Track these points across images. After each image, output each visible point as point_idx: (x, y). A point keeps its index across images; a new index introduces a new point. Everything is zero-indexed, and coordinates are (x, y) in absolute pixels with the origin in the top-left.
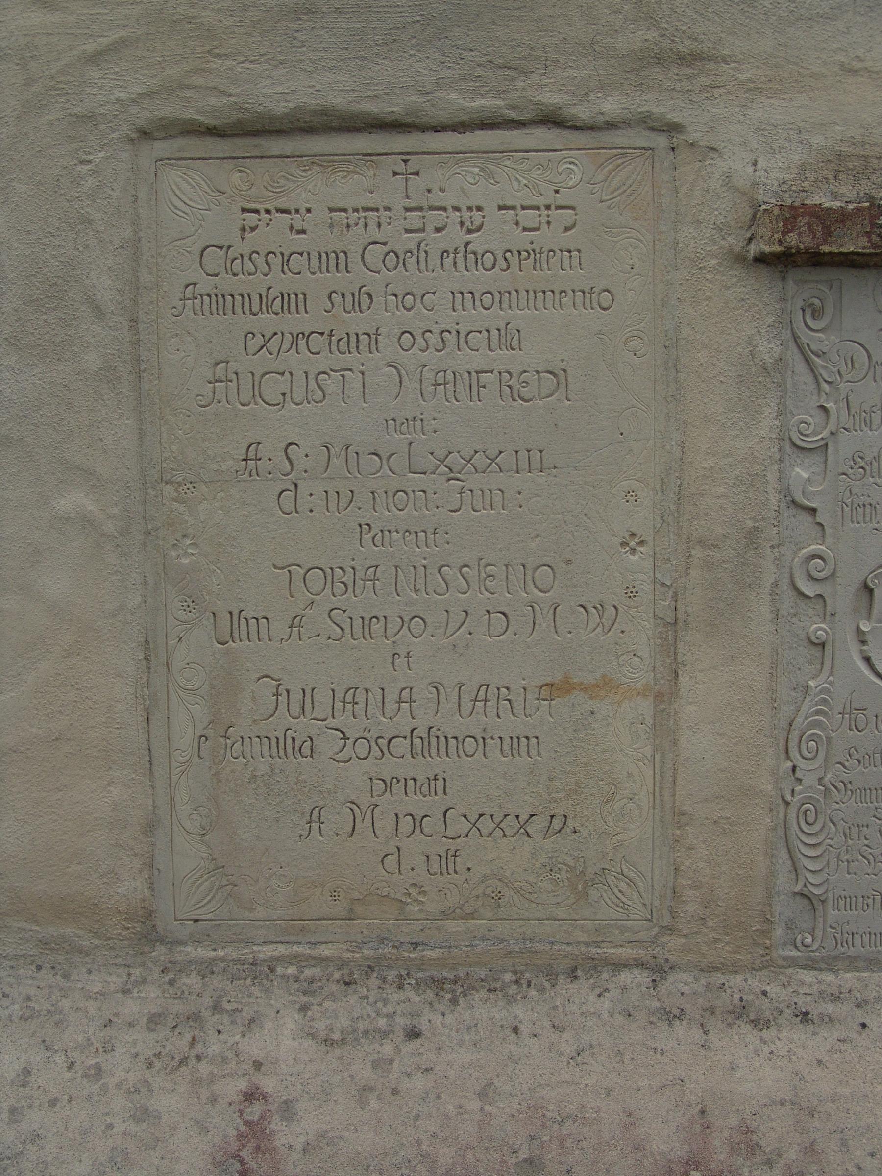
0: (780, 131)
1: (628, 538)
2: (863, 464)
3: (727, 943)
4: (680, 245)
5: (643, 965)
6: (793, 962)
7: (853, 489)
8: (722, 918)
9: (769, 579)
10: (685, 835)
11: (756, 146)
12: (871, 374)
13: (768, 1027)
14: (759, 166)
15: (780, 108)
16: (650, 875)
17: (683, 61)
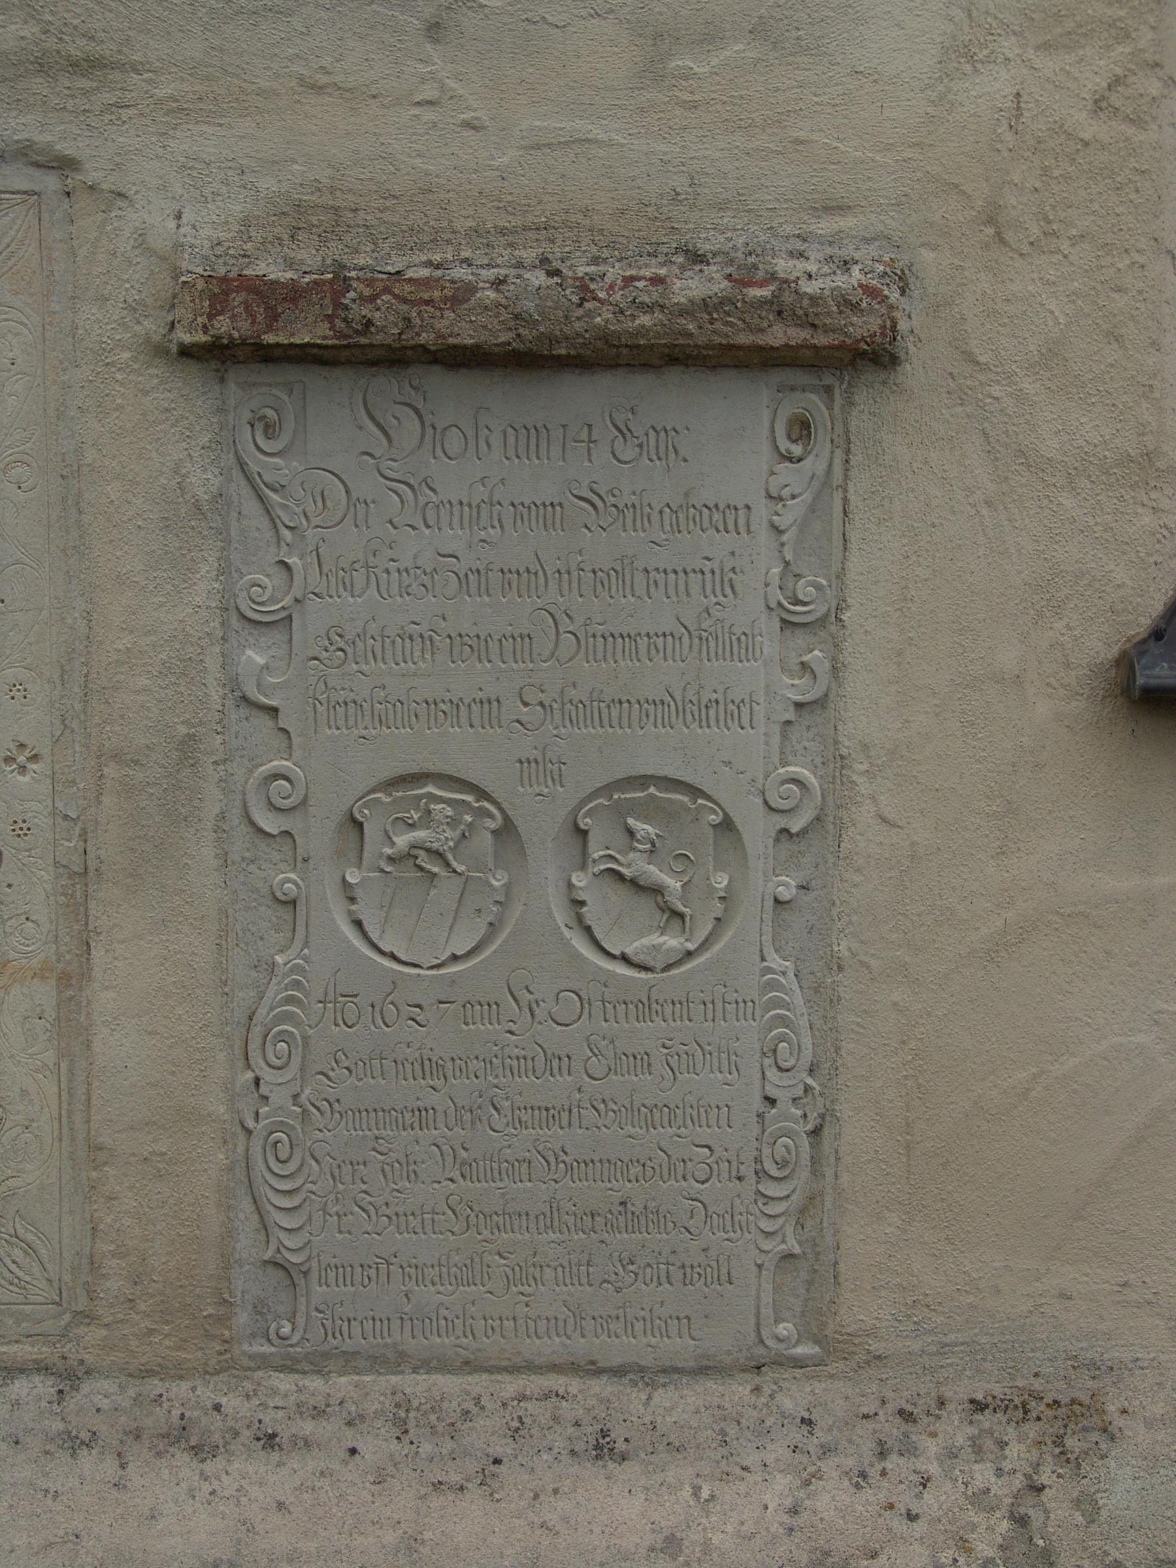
0: (214, 170)
1: (14, 752)
2: (342, 645)
3: (166, 1336)
4: (80, 332)
5: (47, 1369)
6: (264, 1362)
7: (329, 680)
8: (158, 1298)
9: (212, 810)
10: (104, 1179)
11: (180, 191)
12: (350, 516)
13: (214, 1456)
14: (184, 220)
15: (214, 138)
16: (57, 1237)
17: (76, 69)
